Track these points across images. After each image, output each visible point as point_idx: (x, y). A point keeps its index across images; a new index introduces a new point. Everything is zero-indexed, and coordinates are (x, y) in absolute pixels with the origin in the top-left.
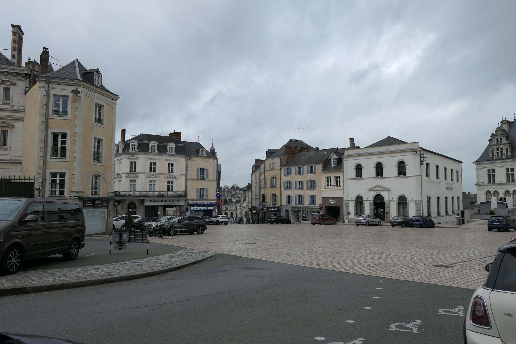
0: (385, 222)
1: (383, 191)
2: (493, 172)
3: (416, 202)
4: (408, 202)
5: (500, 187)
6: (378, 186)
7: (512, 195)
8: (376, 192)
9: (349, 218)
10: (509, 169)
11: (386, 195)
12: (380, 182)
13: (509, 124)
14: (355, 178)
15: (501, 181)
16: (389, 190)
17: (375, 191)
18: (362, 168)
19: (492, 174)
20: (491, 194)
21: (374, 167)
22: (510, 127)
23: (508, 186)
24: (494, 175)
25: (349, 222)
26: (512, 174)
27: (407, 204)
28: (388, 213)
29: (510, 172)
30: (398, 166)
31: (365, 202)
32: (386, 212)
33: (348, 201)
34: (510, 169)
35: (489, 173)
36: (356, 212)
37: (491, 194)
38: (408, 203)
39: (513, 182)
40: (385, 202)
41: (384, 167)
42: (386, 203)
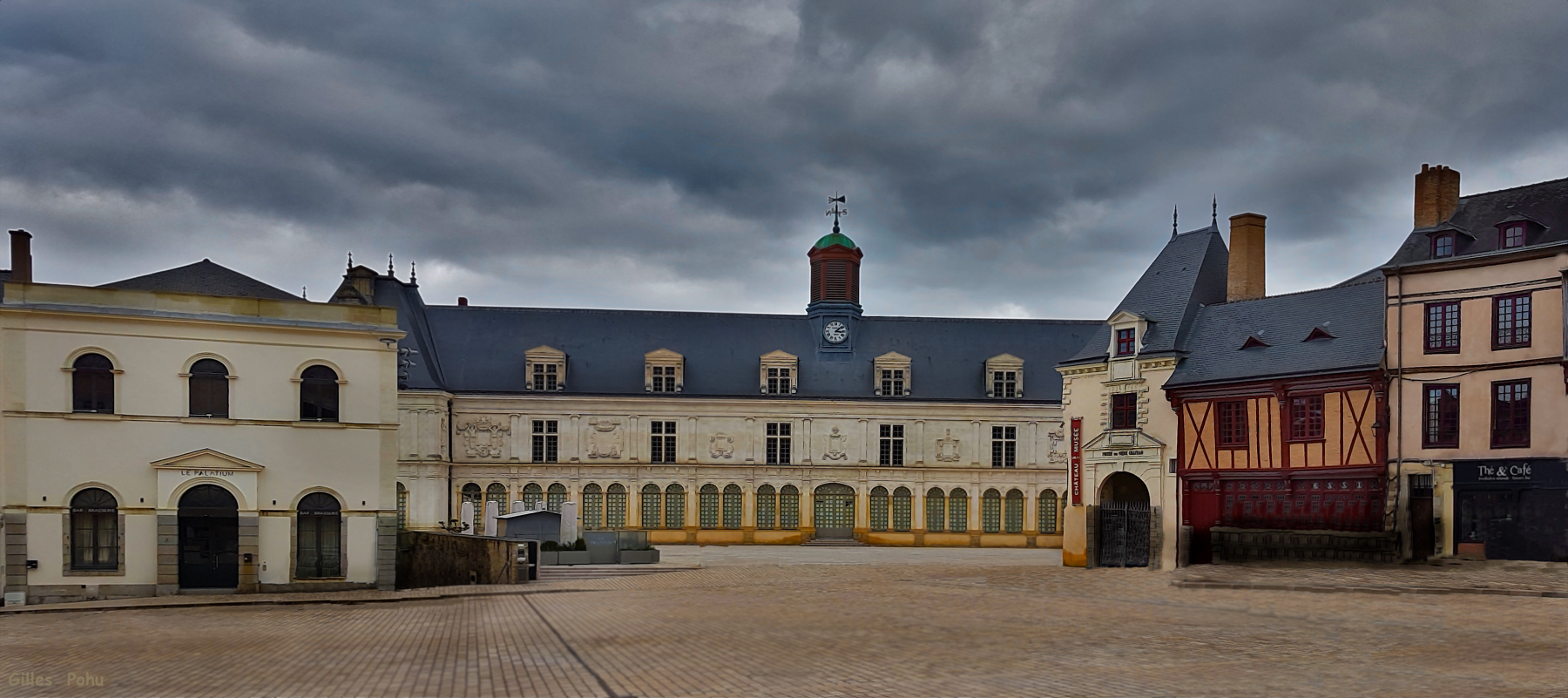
0: (241, 592)
1: (230, 472)
2: (549, 430)
3: (380, 515)
4: (343, 515)
5: (919, 476)
6: (206, 453)
7: (545, 496)
8: (193, 475)
9: (30, 583)
10: (541, 423)
11: (248, 494)
12: (209, 434)
13: (373, 281)
14: (71, 412)
15: (977, 461)
16: (259, 470)
17: (192, 473)
18: (227, 380)
19: (547, 436)
20: (542, 494)
21: (65, 370)
22: (375, 291)
23: (655, 471)
24: (674, 438)
25: (27, 603)
26: (549, 438)
27: (340, 522)
28: (254, 558)
29: (545, 434)
30: (302, 384)
31: (127, 517)
32: (246, 555)
33: (24, 511)
34: (545, 423)
35: (535, 430)
36: (69, 560)
37: (542, 494)
38: (346, 518)
39: (997, 467)
40: (240, 515)
41: (235, 378)
42: (243, 518)
